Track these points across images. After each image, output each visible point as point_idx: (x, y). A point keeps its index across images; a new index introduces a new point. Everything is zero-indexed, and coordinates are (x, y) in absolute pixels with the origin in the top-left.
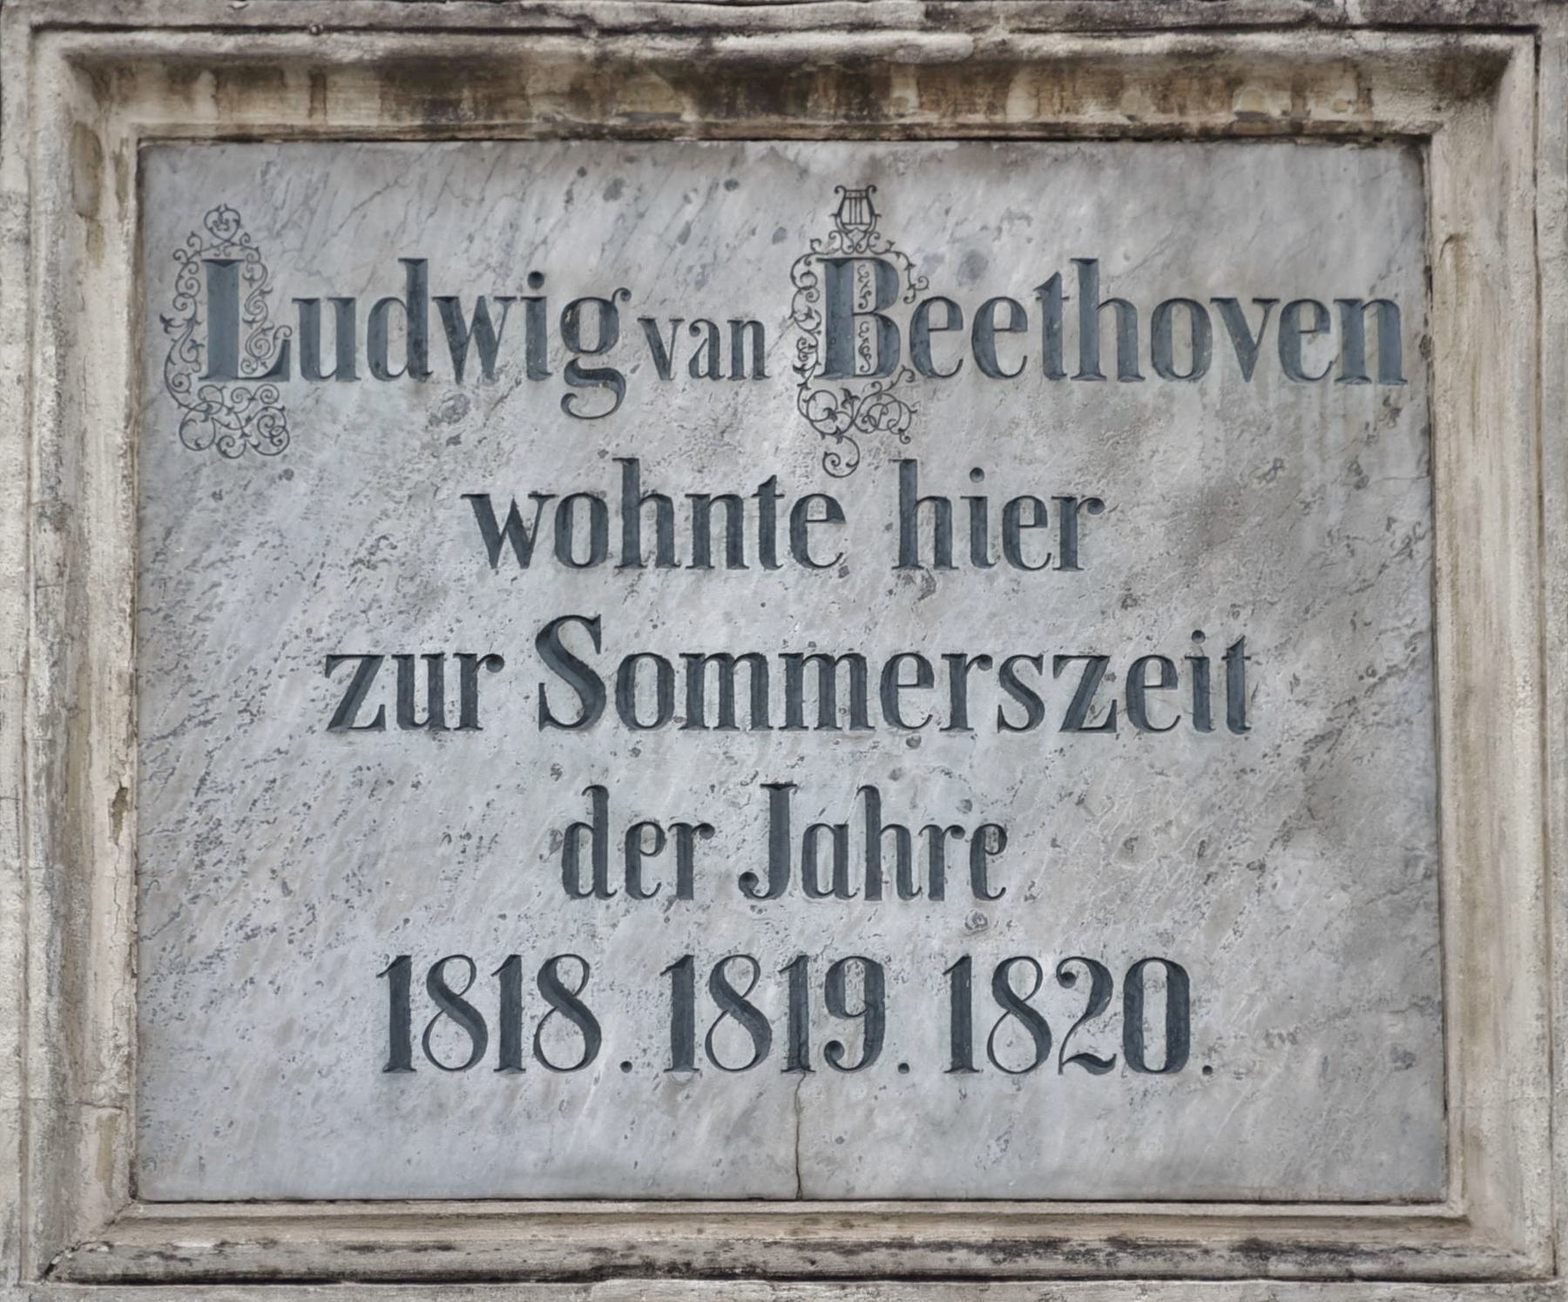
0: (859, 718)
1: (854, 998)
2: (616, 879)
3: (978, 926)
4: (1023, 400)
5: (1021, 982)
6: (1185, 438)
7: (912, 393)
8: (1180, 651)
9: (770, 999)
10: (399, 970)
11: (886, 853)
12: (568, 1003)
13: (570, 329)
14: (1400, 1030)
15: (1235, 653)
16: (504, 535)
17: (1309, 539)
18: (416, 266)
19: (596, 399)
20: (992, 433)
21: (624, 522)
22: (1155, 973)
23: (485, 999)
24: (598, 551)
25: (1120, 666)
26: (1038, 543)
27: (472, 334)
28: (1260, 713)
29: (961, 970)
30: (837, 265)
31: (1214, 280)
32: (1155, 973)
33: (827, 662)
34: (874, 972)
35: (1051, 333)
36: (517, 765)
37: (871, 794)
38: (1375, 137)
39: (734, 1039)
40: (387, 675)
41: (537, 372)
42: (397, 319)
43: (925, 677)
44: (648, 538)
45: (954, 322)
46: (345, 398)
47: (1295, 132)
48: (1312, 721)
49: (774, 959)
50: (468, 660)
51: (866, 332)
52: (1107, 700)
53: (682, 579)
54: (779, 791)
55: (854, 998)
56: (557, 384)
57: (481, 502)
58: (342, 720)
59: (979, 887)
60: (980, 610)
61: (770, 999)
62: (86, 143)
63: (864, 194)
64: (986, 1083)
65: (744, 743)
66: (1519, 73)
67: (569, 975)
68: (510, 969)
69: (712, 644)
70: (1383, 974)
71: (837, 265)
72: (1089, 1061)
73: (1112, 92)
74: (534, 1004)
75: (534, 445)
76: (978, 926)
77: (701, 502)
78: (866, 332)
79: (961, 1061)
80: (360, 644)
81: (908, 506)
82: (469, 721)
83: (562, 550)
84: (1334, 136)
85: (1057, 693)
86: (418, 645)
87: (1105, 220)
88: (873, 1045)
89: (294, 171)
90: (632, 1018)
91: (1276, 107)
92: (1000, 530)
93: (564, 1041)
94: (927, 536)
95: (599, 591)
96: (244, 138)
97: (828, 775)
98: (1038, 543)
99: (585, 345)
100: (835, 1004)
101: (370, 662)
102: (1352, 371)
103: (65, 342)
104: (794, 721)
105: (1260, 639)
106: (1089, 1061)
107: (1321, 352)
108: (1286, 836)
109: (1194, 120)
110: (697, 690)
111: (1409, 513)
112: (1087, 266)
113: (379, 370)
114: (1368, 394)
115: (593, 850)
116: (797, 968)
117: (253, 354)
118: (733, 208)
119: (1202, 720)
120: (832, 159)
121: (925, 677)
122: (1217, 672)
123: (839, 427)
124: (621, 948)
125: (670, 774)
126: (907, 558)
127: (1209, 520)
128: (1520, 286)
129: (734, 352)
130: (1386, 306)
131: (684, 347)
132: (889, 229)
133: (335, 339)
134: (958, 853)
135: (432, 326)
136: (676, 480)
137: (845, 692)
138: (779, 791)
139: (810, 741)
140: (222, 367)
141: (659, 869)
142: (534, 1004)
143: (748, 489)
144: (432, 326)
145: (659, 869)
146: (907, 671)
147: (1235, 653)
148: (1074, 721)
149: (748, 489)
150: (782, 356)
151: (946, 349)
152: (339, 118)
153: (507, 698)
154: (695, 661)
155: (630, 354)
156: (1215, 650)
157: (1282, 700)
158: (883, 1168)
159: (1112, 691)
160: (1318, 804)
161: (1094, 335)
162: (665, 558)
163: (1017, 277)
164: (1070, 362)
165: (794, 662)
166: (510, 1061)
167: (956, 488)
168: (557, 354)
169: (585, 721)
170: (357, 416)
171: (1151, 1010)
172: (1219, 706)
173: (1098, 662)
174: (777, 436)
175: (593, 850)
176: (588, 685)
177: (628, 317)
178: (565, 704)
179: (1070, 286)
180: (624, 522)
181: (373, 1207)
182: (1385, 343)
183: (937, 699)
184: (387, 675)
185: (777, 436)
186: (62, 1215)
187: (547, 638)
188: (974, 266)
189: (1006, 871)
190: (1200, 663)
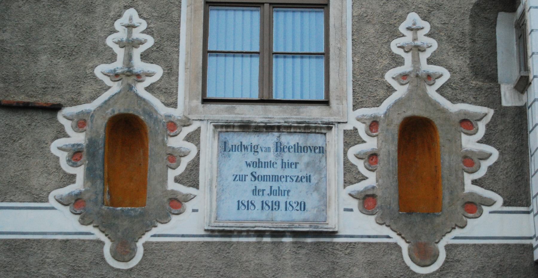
0: (278, 181)
1: (277, 204)
2: (257, 194)
3: (288, 198)
4: (292, 154)
5: (291, 203)
6: (306, 157)
7: (283, 153)
8: (305, 175)
9: (270, 204)
10: (239, 201)
11: (280, 192)
12: (253, 204)
13: (254, 148)
14: (323, 208)
15: (310, 176)
16: (248, 165)
17: (316, 166)
18: (241, 142)
19: (256, 153)
20: (288, 157)
21: (258, 164)
22: (303, 203)
23: (246, 204)
24: (256, 166)
25: (300, 177)
26: (293, 166)
27: (246, 148)
28: (312, 181)
29: (286, 202)
30: (277, 143)
31: (308, 145)
32: (303, 203)
33: (275, 176)
34: (279, 202)
35: (295, 149)
36: (249, 184)
37: (279, 187)
38: (322, 133)
39: (267, 208)
40: (238, 177)
41: (251, 151)
42: (240, 147)
43: (284, 177)
44: (260, 165)
45: (292, 147)
46: (235, 153)
47: (315, 133)
48: (316, 182)
49: (270, 201)
50: (245, 176)
51: (279, 148)
52: (299, 180)
53: (263, 168)
54: (271, 187)
55: (277, 204)
56: (253, 152)
57: (246, 162)
58: (234, 180)
59: (288, 195)
60: (288, 172)
61: (270, 204)
62: (214, 131)
63: (279, 137)
64: (288, 211)
65: (268, 182)
66: (334, 128)
67: (253, 202)
68: (248, 202)
69: (265, 174)
70: (322, 203)
71: (277, 143)
72: (297, 210)
73: (300, 129)
74: (250, 204)
75: (251, 157)
76: (288, 198)
77: (265, 162)
78: (279, 148)
79: (286, 210)
80: (236, 174)
81: (282, 163)
82: (245, 180)
83: (253, 166)
84: (318, 133)
85: (295, 179)
86: (241, 174)
87: (299, 140)
88: (279, 209)
89: (232, 134)
90: (258, 206)
91: (314, 130)
92: (290, 165)
93: (252, 207)
94: (284, 165)
95: (256, 170)
96: (227, 132)
97: (275, 185)
98: (293, 166)
99: (255, 149)
100: (275, 205)
101: (237, 175)
102: (320, 153)
103: (212, 148)
104: (272, 181)
105: (312, 174)
106: (297, 210)
107: (317, 151)
108: (314, 191)
109: (307, 131)
110: (264, 178)
111: (324, 164)
112: (298, 143)
113: (238, 151)
114: (321, 154)
115: (255, 192)
116: (272, 202)
117: (227, 150)
118: (268, 138)
119: (307, 181)
120: (277, 134)
121: (284, 177)
122: (308, 178)
123: (277, 156)
124: (258, 200)
125: (262, 185)
126: (282, 167)
127: (308, 164)
128: (334, 146)
129: (268, 150)
130: (323, 147)
131: (264, 150)
132: (281, 140)
133: (234, 148)
134: (286, 192)
135: (242, 147)
136: (263, 160)
137: (277, 178)
138: (271, 187)
139: (274, 182)
140: (225, 150)
141: (261, 193)
142: (250, 204)
143: (269, 161)
144: (242, 147)
145: (261, 193)
146: (282, 177)
147: (310, 176)
148: (296, 181)
149: (269, 161)
150: (272, 150)
151: (286, 150)
152: (235, 130)
153: (248, 178)
154: (264, 176)
155: (259, 150)
156: (308, 175)
157: (314, 179)
158: (279, 219)
159: (299, 179)
160: (317, 189)
161: (299, 149)
162: (262, 167)
163: (292, 144)
164: (296, 151)
165: (273, 176)
166: (248, 209)
167: (286, 162)
168: (253, 150)
169: (255, 180)
170: (236, 155)
171: (302, 206)
172: (308, 180)
173: (298, 177)
174: (271, 156)
175: (255, 192)
176: (255, 178)
177: (259, 147)
178: (253, 179)
179: (296, 145)
180: (258, 164)
181: (237, 221)
182: (322, 150)
183: (285, 179)
184: (238, 177)
185: (271, 156)
186: (210, 222)
187: (252, 174)
188: (288, 143)
189: (290, 194)
190: (307, 177)
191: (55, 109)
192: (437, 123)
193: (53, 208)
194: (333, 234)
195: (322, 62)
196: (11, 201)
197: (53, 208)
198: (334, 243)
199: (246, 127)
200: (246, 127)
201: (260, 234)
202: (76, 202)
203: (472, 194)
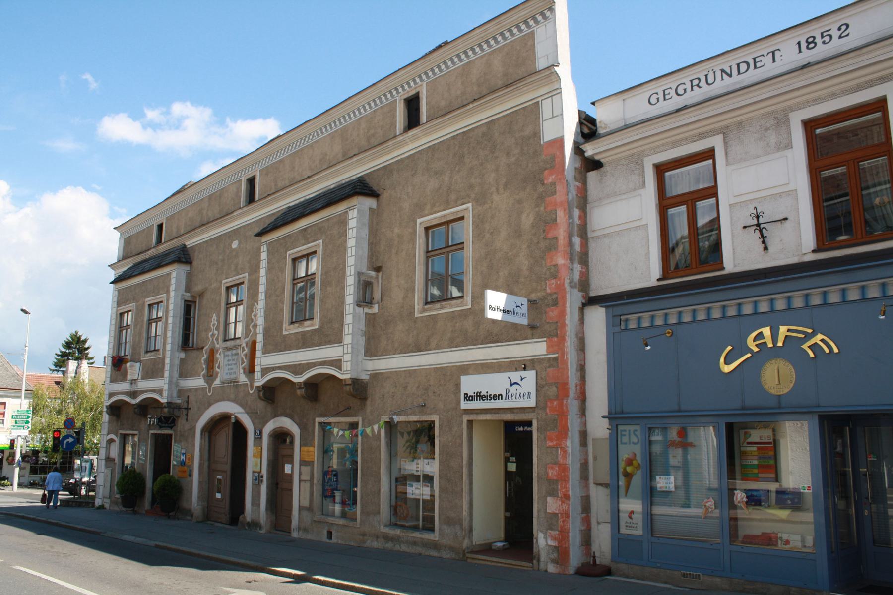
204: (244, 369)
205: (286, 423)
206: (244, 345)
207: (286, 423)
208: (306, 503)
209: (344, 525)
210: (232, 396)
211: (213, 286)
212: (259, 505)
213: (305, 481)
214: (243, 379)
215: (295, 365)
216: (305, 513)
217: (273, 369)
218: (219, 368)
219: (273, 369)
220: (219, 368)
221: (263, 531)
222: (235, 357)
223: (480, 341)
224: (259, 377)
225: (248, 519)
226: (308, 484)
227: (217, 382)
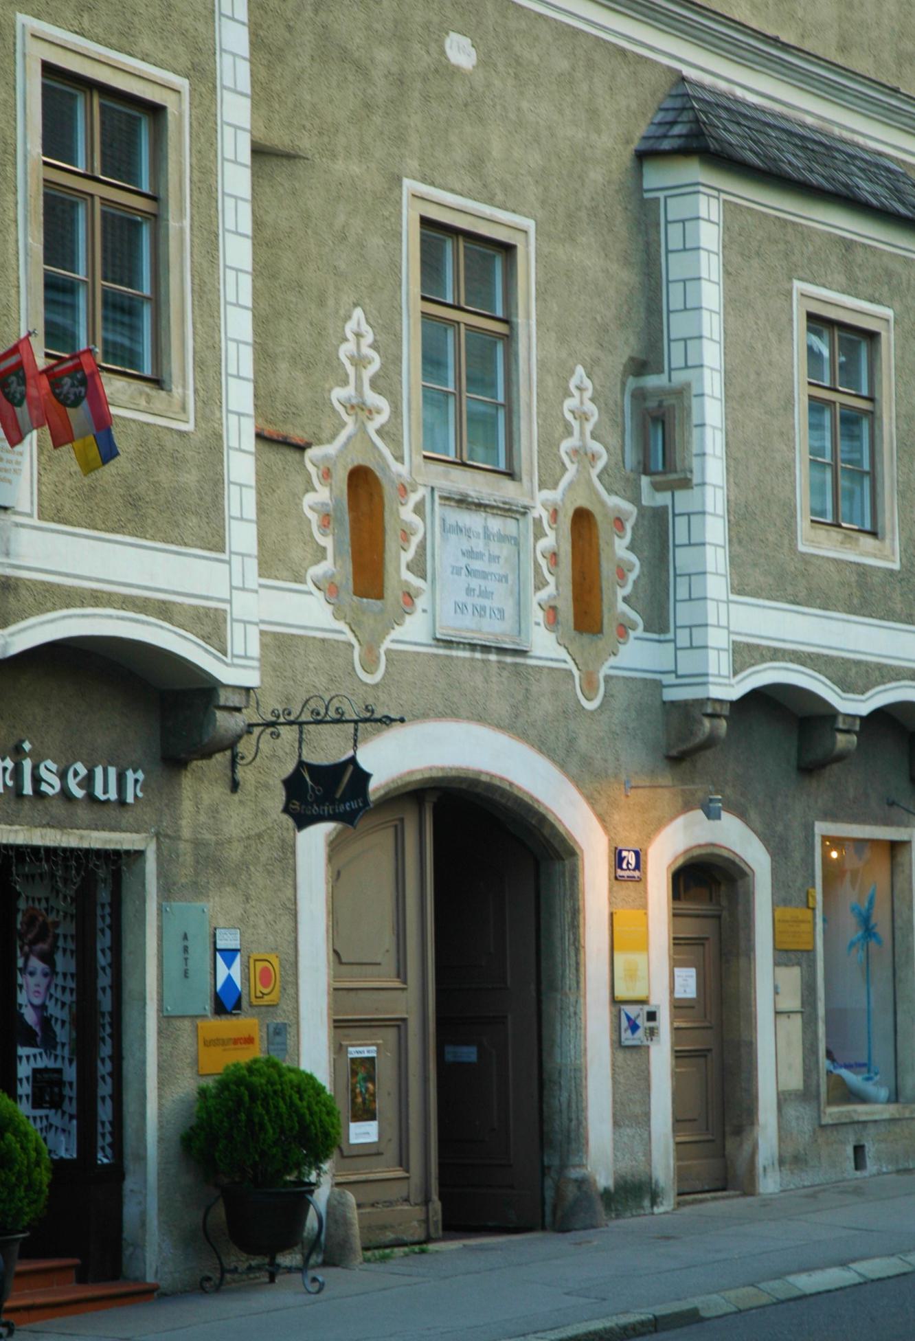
11: (485, 594)
191: (301, 448)
192: (599, 518)
193: (310, 593)
194: (522, 653)
195: (694, 630)
196: (276, 578)
197: (310, 593)
198: (527, 666)
199: (463, 502)
200: (463, 502)
201: (486, 649)
202: (330, 589)
203: (624, 614)
204: (552, 613)
205: (735, 837)
206: (539, 512)
207: (735, 837)
208: (795, 1081)
209: (893, 1121)
210: (500, 708)
211: (339, 166)
212: (644, 1119)
213: (788, 1013)
214: (545, 646)
215: (846, 661)
216: (791, 1111)
217: (776, 654)
218: (418, 567)
219: (776, 654)
220: (418, 567)
221: (666, 1205)
222: (505, 550)
223: (545, 671)
224: (726, 669)
225: (604, 1180)
226: (797, 1021)
227: (412, 632)
